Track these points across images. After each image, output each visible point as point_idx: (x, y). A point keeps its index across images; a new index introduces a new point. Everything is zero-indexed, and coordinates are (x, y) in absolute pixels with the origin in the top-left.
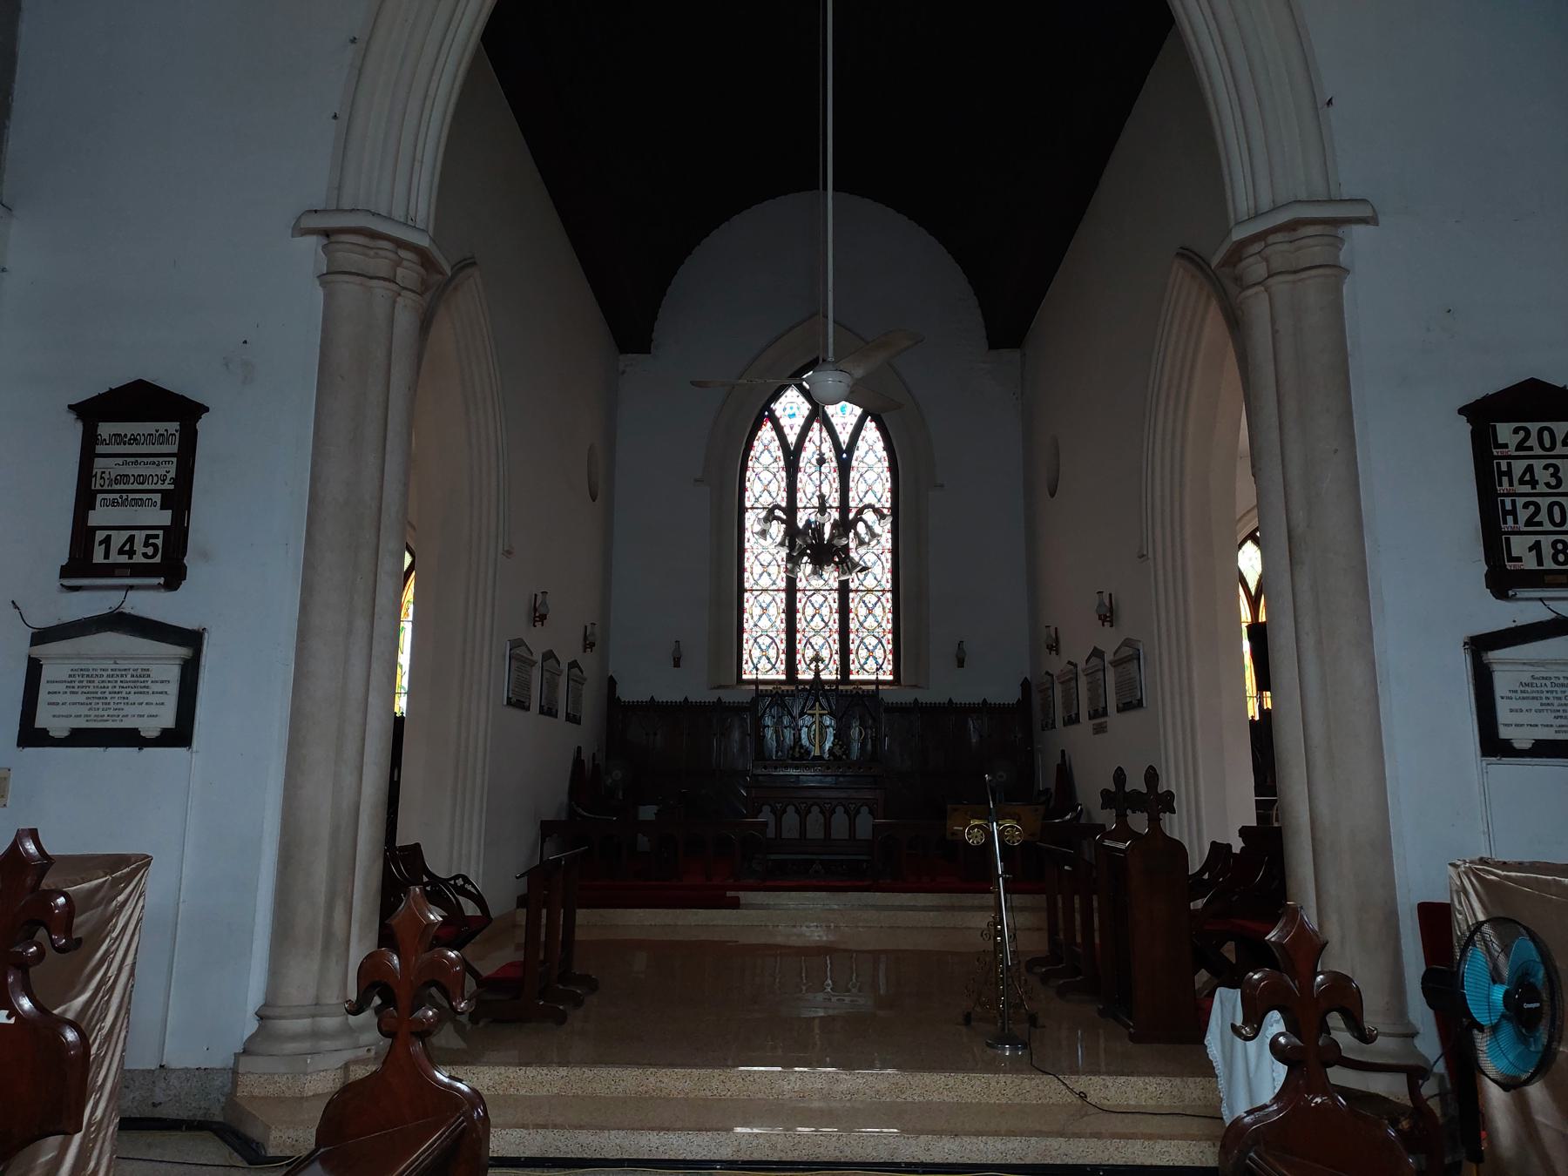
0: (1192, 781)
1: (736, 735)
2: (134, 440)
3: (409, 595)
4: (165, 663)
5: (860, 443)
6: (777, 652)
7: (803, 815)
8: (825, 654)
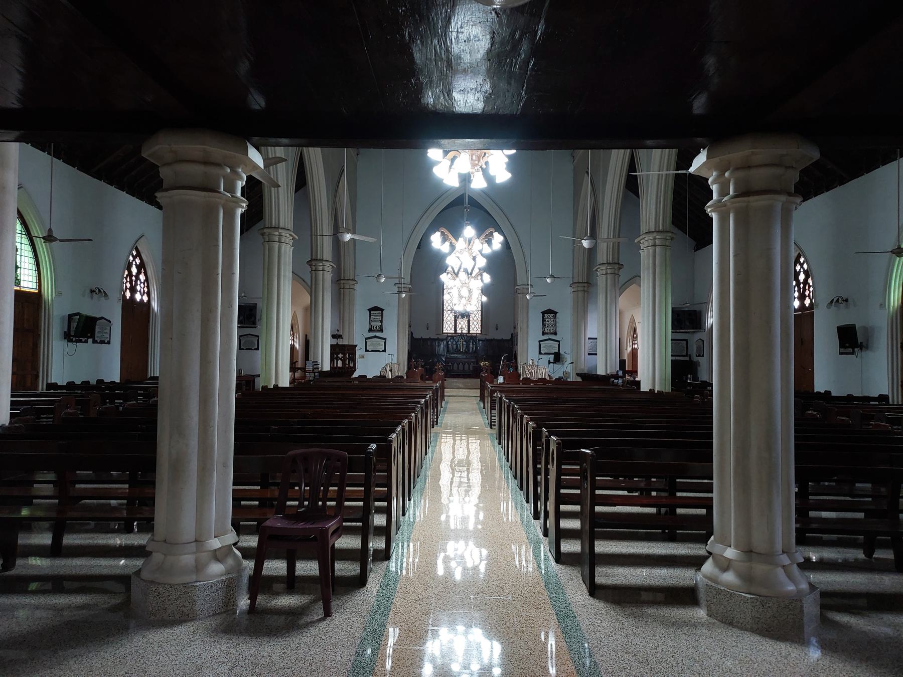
1: (442, 346)
7: (458, 365)
8: (464, 326)
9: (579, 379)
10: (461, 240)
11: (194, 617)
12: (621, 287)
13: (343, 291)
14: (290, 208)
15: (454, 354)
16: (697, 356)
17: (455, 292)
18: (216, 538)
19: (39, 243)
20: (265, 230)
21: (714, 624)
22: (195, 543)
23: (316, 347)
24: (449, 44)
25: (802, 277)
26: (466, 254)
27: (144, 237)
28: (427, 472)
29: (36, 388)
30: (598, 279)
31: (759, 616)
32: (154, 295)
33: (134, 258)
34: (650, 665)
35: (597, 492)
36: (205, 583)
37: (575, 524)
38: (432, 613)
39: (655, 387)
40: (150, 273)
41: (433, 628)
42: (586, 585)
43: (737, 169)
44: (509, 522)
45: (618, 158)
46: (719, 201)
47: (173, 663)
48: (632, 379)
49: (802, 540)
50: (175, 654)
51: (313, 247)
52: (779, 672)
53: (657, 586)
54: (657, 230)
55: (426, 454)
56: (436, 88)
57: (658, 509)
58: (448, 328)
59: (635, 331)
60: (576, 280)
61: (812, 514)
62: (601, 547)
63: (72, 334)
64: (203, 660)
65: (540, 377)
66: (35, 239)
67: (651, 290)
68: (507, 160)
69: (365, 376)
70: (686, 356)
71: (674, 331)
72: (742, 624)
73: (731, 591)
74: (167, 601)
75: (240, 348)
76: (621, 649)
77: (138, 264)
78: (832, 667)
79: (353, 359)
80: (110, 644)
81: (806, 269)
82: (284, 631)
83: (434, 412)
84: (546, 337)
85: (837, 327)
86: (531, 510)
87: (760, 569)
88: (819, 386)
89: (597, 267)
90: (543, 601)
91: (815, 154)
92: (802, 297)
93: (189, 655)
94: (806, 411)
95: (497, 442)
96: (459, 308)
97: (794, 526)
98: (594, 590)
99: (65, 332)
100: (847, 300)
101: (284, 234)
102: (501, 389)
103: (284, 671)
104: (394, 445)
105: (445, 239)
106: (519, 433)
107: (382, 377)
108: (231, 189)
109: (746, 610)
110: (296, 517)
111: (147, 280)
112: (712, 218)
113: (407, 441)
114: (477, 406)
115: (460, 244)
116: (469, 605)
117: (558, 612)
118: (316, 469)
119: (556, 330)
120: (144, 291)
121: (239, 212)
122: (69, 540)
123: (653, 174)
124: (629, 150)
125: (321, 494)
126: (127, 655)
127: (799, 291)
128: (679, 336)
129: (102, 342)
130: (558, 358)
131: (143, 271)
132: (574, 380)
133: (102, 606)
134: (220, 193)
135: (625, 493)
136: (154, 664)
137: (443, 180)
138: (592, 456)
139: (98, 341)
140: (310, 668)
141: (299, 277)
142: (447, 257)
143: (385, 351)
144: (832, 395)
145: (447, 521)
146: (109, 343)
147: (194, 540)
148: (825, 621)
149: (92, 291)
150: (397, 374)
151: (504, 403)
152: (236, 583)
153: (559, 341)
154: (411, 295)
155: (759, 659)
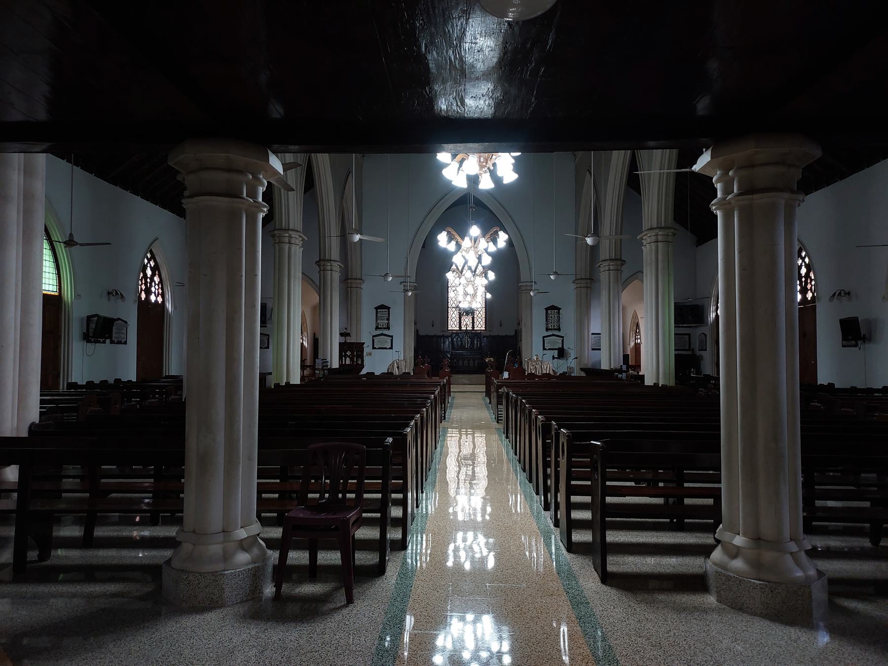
0: (67, 332)
1: (447, 343)
2: (382, 312)
3: (852, 488)
4: (389, 339)
5: (477, 270)
6: (457, 323)
8: (468, 323)
9: (583, 374)
10: (467, 239)
11: (222, 604)
12: (624, 282)
13: (351, 290)
14: (299, 208)
15: (459, 350)
16: (699, 350)
17: (460, 290)
18: (242, 529)
19: (61, 249)
20: (276, 232)
21: (724, 609)
22: (222, 533)
23: (325, 345)
24: (463, 54)
25: (804, 271)
26: (472, 253)
27: (158, 240)
28: (436, 465)
29: (57, 387)
30: (601, 276)
31: (768, 602)
32: (168, 296)
33: (149, 260)
34: (663, 649)
35: (608, 483)
36: (232, 571)
37: (586, 515)
38: (450, 600)
39: (659, 381)
40: (164, 277)
41: (451, 614)
42: (597, 573)
43: (741, 168)
44: (518, 514)
45: (618, 159)
46: (724, 199)
47: (206, 647)
48: (636, 373)
49: (809, 530)
50: (207, 638)
51: (322, 249)
52: (789, 655)
53: (667, 574)
54: (659, 226)
55: (436, 448)
56: (450, 94)
57: (665, 499)
58: (453, 325)
59: (638, 326)
60: (579, 277)
61: (819, 503)
62: (612, 537)
63: (91, 335)
64: (235, 644)
65: (544, 372)
66: (56, 244)
67: (654, 284)
68: (513, 161)
69: (374, 373)
70: (689, 350)
71: (677, 325)
72: (751, 609)
73: (740, 578)
74: (196, 589)
75: (261, 348)
76: (634, 633)
77: (152, 266)
78: (841, 650)
79: (361, 357)
80: (146, 629)
81: (807, 263)
82: (309, 618)
83: (441, 408)
84: (550, 333)
85: (840, 320)
86: (541, 502)
87: (768, 556)
88: (823, 377)
89: (600, 264)
90: (557, 588)
91: (817, 153)
92: (804, 291)
93: (221, 639)
94: (58, 579)
95: (504, 436)
96: (464, 305)
97: (801, 514)
98: (607, 578)
99: (84, 333)
100: (849, 294)
101: (293, 236)
102: (506, 384)
103: (311, 654)
104: (409, 438)
105: (450, 238)
106: (527, 426)
107: (389, 374)
108: (253, 194)
109: (756, 596)
110: (316, 506)
111: (161, 282)
112: (717, 215)
113: (419, 435)
114: (483, 401)
115: (466, 243)
116: (485, 593)
117: (572, 598)
118: (335, 461)
119: (559, 325)
120: (158, 292)
121: (261, 216)
122: (100, 532)
123: (654, 173)
124: (629, 151)
125: (341, 486)
126: (162, 639)
127: (801, 284)
128: (682, 331)
129: (119, 342)
130: (562, 353)
131: (157, 273)
132: (578, 375)
133: (135, 594)
134: (243, 198)
135: (633, 484)
136: (189, 647)
137: (452, 181)
138: (602, 447)
139: (116, 342)
140: (336, 651)
141: (309, 277)
142: (453, 256)
143: (392, 349)
144: (836, 387)
145: (455, 513)
146: (125, 343)
147: (221, 530)
148: (833, 607)
149: (109, 293)
150: (404, 371)
151: (512, 398)
152: (262, 572)
153: (563, 337)
154: (416, 293)
155: (770, 643)
